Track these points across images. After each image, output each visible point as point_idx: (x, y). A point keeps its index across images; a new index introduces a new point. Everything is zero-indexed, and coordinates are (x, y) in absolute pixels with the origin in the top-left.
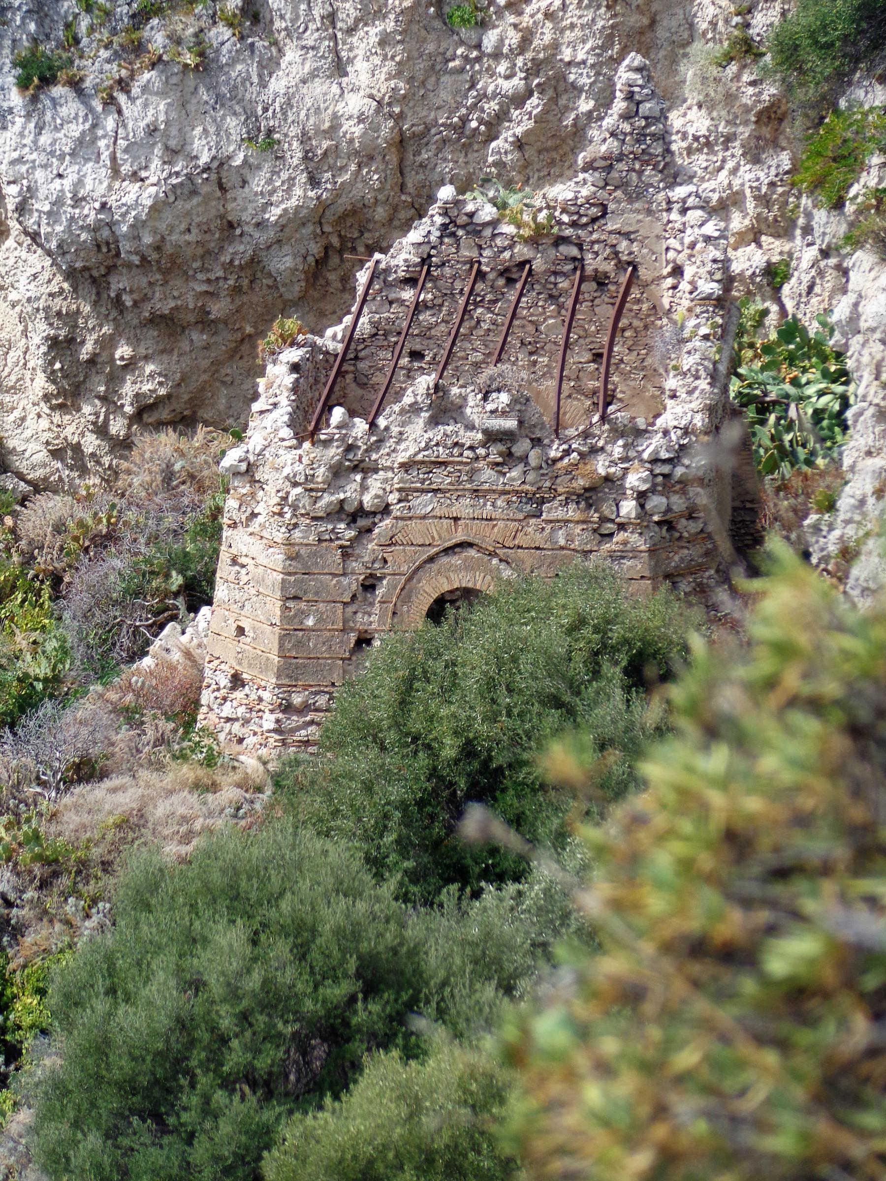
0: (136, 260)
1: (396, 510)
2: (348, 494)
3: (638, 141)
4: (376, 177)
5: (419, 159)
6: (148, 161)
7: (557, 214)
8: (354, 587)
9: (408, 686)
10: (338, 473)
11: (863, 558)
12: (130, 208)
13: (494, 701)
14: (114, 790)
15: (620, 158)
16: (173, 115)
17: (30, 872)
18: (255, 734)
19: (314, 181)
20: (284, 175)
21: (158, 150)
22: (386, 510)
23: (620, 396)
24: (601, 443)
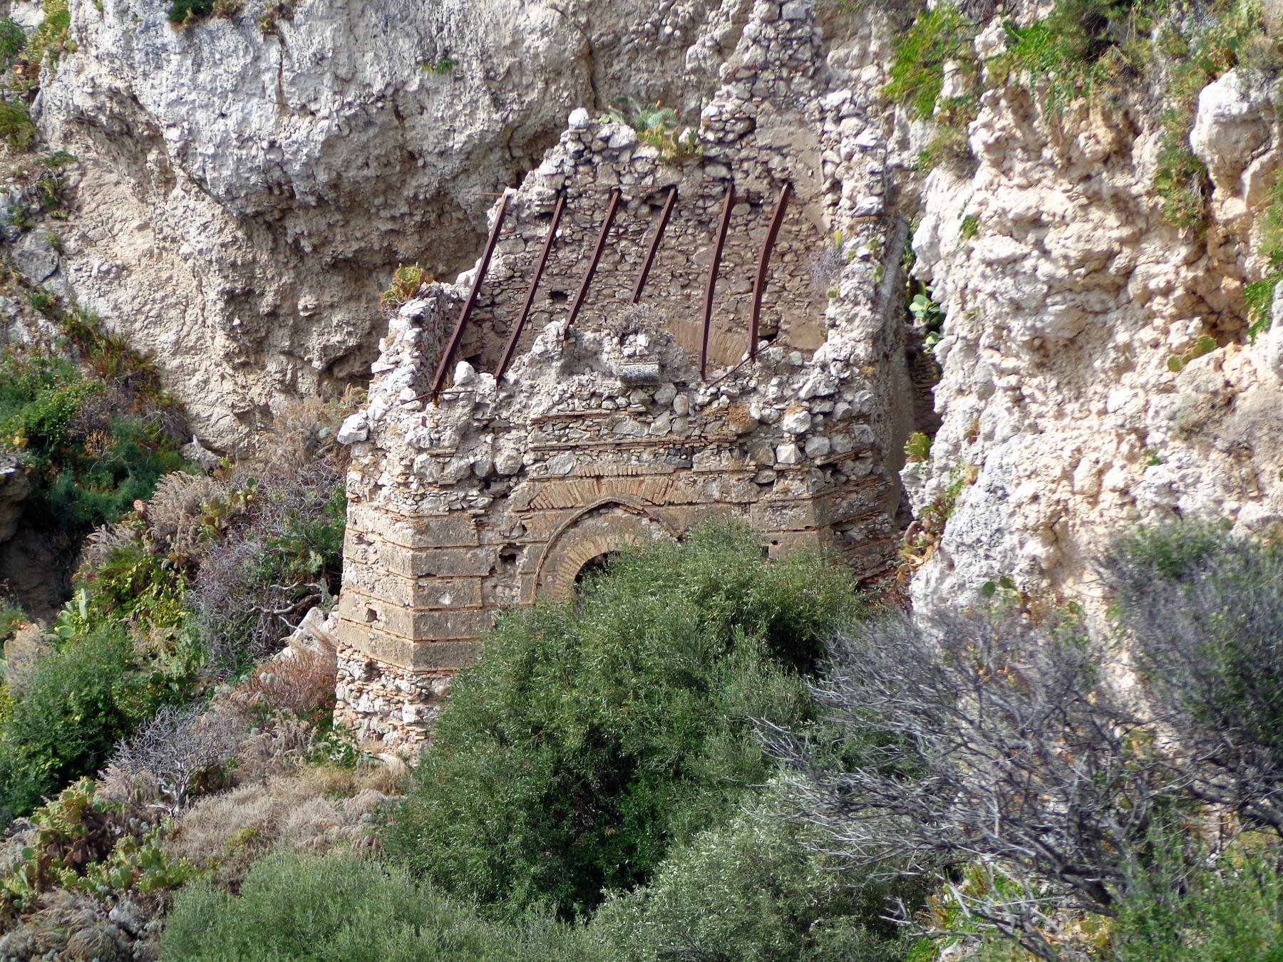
0: (312, 200)
1: (533, 471)
2: (479, 458)
3: (784, 47)
4: (565, 94)
5: (611, 71)
6: (317, 91)
7: (701, 132)
8: (492, 558)
9: (528, 668)
10: (466, 434)
11: (956, 509)
12: (301, 145)
13: (619, 682)
14: (243, 801)
15: (765, 67)
16: (341, 40)
17: (153, 898)
18: (395, 728)
19: (497, 103)
20: (466, 98)
21: (327, 79)
22: (522, 472)
23: (785, 327)
24: (753, 384)
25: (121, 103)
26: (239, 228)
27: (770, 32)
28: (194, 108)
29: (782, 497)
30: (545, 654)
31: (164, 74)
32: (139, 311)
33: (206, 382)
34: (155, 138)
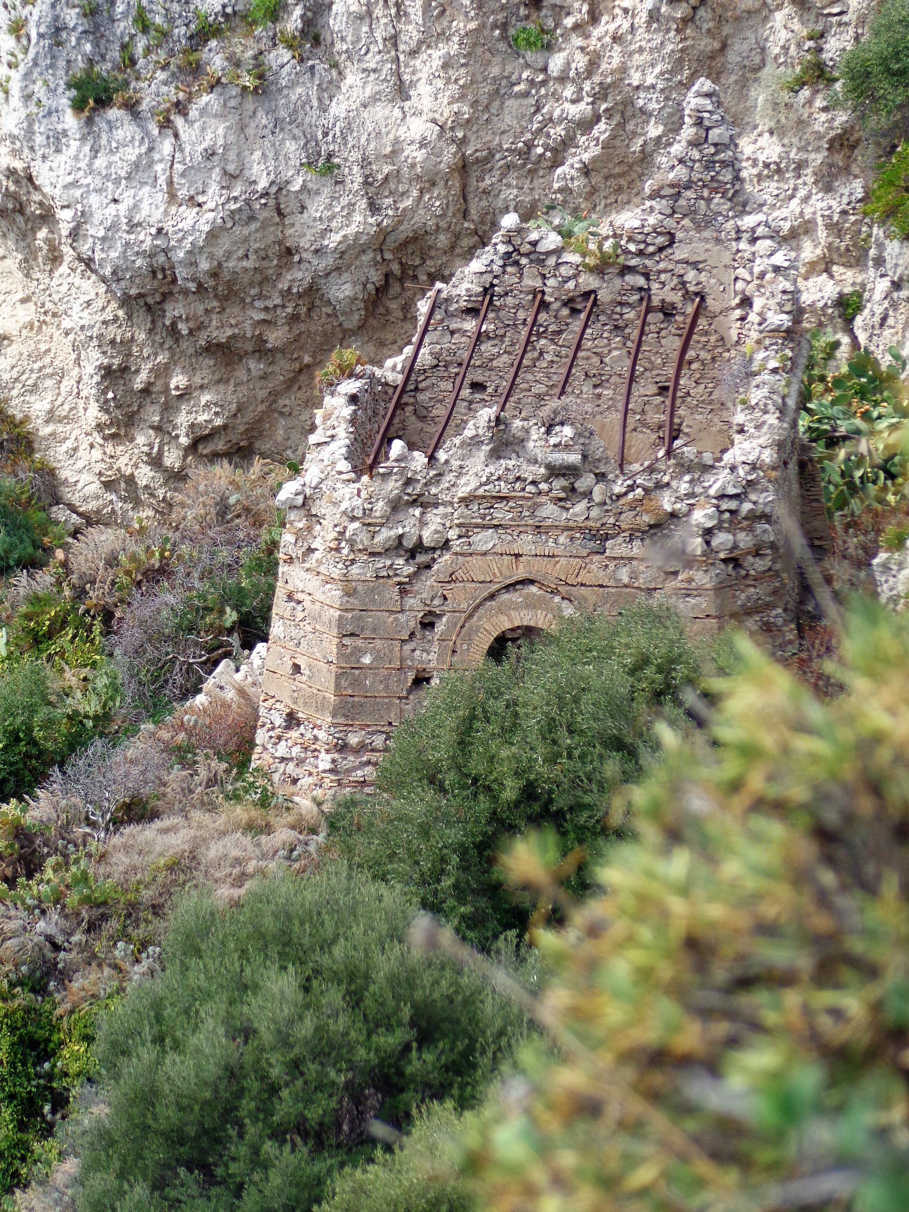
0: (192, 286)
1: (456, 545)
2: (407, 529)
3: (707, 168)
5: (482, 185)
7: (623, 243)
8: (412, 624)
10: (396, 506)
13: (554, 742)
14: (165, 831)
16: (232, 138)
17: (78, 914)
19: (374, 208)
20: (344, 201)
21: (216, 174)
23: (686, 430)
24: (666, 479)
25: (17, 182)
26: (121, 307)
27: (696, 155)
28: (88, 192)
29: (686, 585)
30: (485, 711)
31: (61, 158)
32: (17, 380)
33: (75, 449)
34: (47, 217)
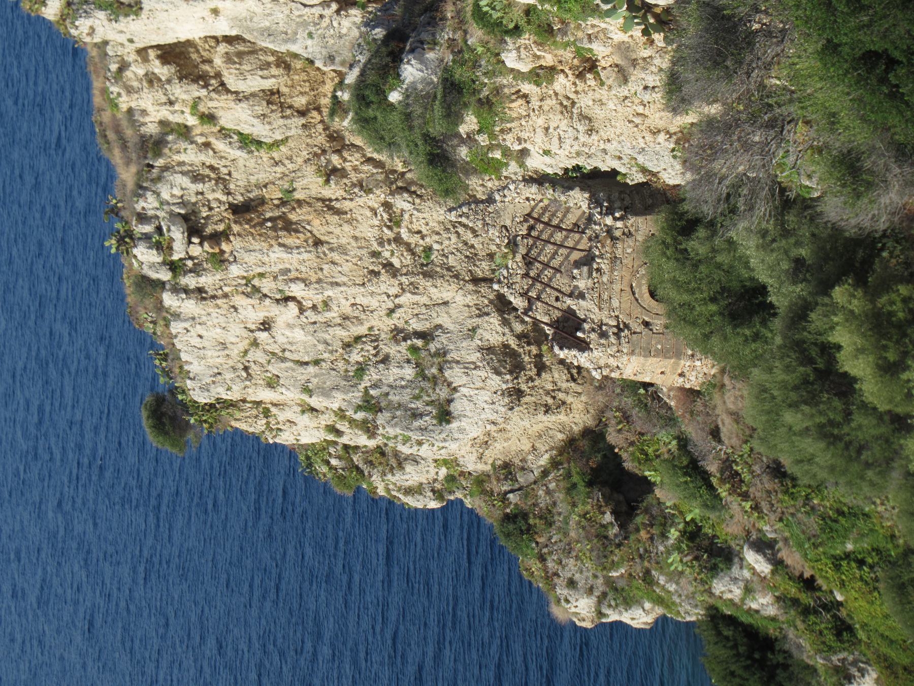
14: (723, 423)
19: (487, 314)
